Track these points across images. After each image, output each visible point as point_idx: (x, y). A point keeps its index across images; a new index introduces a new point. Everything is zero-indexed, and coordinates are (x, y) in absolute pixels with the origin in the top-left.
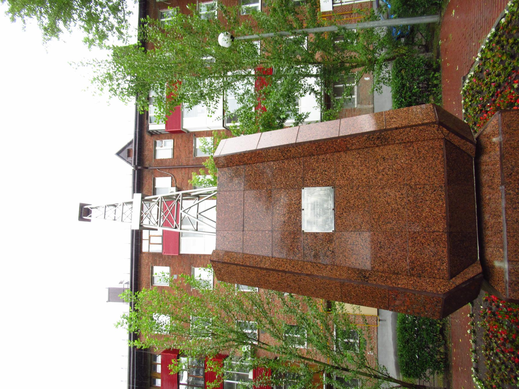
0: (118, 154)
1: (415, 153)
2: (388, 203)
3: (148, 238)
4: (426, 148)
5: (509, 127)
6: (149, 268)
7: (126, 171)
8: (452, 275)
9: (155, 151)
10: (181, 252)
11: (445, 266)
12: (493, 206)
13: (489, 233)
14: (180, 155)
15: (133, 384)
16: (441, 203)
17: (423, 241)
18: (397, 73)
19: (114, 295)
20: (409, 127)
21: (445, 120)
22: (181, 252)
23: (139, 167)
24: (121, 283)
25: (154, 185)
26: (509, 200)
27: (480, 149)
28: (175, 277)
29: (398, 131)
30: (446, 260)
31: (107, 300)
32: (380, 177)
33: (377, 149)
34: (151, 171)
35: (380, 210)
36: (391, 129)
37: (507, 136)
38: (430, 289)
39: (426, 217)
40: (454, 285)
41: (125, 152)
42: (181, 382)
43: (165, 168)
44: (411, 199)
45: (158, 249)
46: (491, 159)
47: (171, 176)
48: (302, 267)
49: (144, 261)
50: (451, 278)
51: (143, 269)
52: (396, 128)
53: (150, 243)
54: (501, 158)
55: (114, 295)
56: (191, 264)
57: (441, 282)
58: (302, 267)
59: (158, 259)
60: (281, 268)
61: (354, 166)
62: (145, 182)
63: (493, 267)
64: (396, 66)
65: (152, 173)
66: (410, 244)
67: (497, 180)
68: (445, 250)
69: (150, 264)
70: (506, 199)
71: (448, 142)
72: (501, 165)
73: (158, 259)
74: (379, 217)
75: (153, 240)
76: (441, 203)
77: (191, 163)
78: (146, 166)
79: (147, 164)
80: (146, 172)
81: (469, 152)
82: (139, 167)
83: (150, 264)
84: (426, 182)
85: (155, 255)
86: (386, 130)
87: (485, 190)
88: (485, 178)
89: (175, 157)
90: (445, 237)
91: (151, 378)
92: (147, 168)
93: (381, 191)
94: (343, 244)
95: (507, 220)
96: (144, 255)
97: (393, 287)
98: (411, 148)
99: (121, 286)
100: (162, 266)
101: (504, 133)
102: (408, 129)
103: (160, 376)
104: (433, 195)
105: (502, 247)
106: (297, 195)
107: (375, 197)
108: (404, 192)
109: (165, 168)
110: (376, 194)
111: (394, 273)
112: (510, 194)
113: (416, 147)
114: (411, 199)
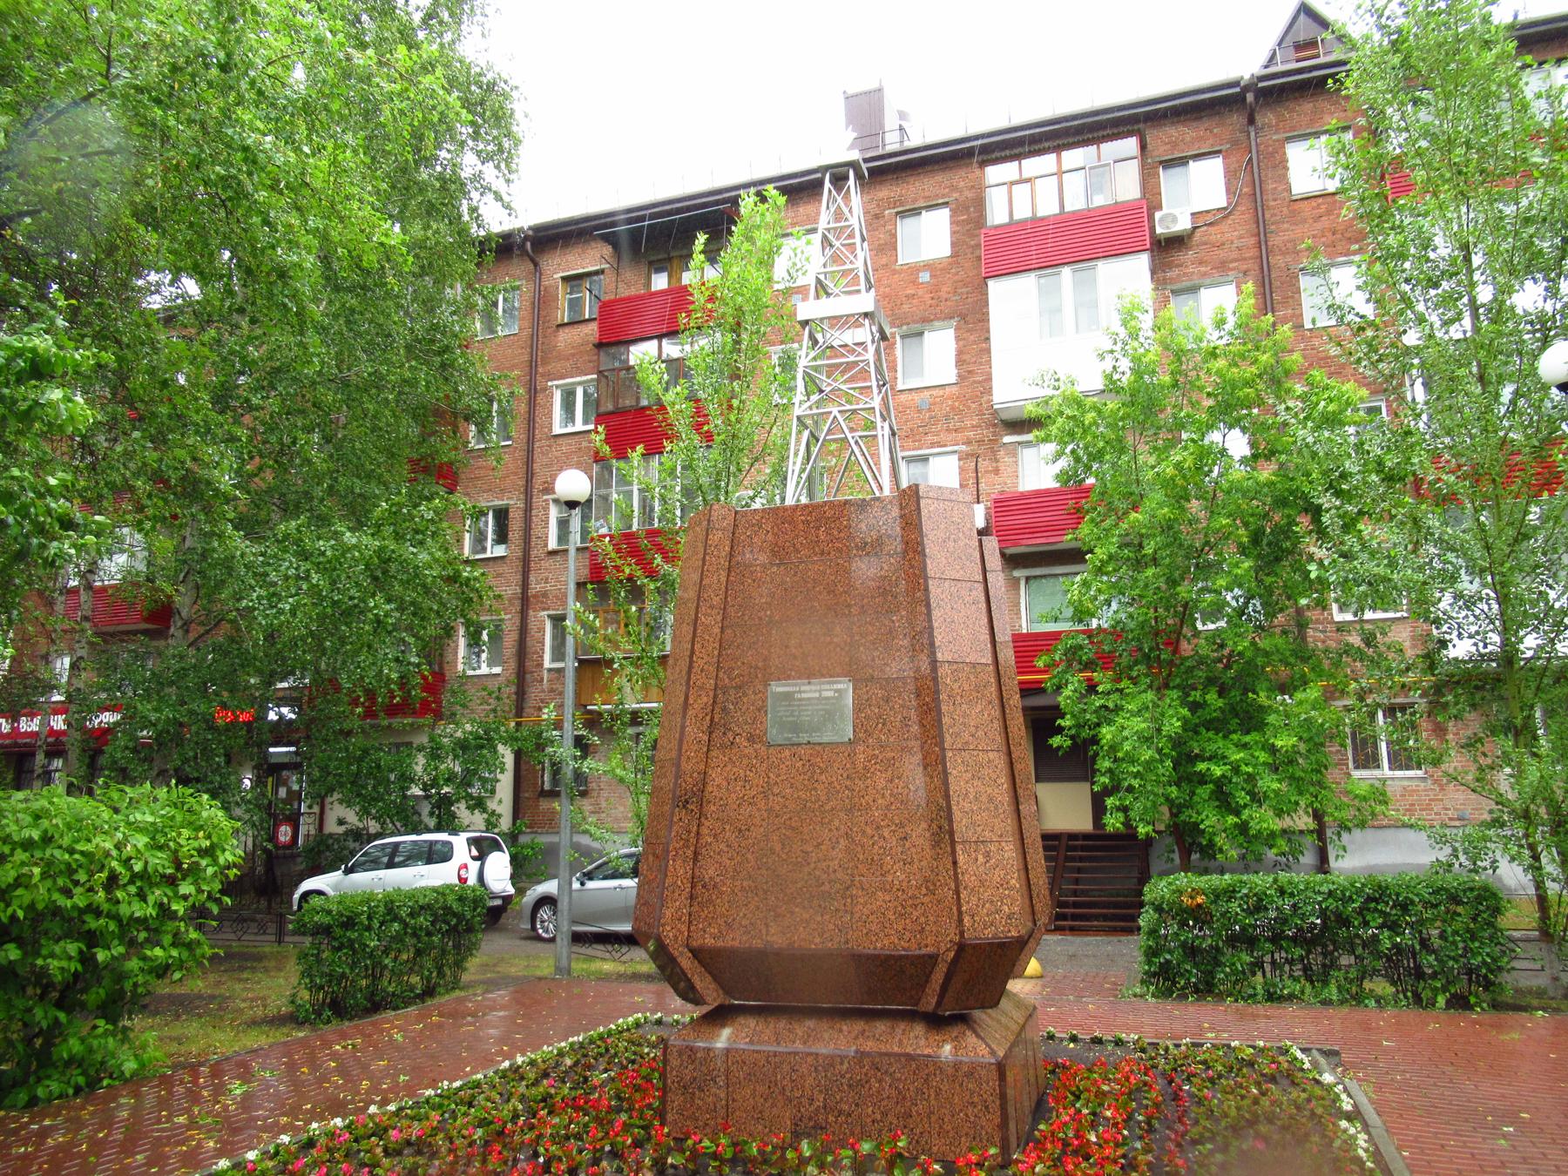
0: (1306, 10)
1: (914, 897)
2: (820, 844)
3: (1025, 176)
4: (923, 919)
5: (970, 1074)
6: (943, 196)
7: (1242, 52)
8: (696, 953)
9: (1317, 135)
10: (991, 283)
11: (709, 941)
12: (826, 1036)
13: (782, 1024)
14: (1304, 221)
15: (652, 217)
16: (817, 940)
17: (752, 906)
18: (1446, 890)
19: (865, 110)
20: (957, 887)
21: (1003, 958)
22: (991, 283)
23: (1250, 97)
24: (902, 115)
25: (1197, 157)
26: (831, 1061)
27: (937, 1022)
28: (925, 277)
29: (950, 866)
30: (720, 944)
31: (851, 92)
32: (869, 831)
33: (924, 825)
34: (1242, 136)
35: (806, 830)
36: (954, 852)
37: (950, 1071)
38: (668, 913)
39: (792, 913)
40: (676, 954)
41: (1305, 29)
42: (664, 341)
43: (1257, 182)
44: (827, 887)
45: (997, 215)
46: (914, 1040)
47: (1229, 204)
48: (701, 688)
49: (959, 178)
50: (691, 951)
51: (939, 177)
52: (955, 863)
53: (1013, 183)
54: (908, 1055)
55: (865, 110)
56: (963, 317)
57: (682, 933)
58: (701, 688)
59: (970, 215)
60: (697, 646)
61: (891, 781)
62: (1206, 123)
63: (723, 1026)
64: (1472, 889)
65: (1235, 143)
66: (745, 884)
67: (869, 1046)
68: (736, 944)
69: (955, 195)
70: (832, 1057)
71: (933, 959)
72: (896, 1055)
73: (970, 215)
74: (793, 829)
75: (1021, 191)
76: (817, 940)
77: (1278, 260)
78: (1257, 117)
79: (1266, 118)
80: (1237, 119)
81: (924, 1000)
82: (1250, 97)
83: (955, 195)
84: (857, 916)
85: (980, 203)
86: (953, 843)
87: (859, 1025)
88: (881, 1027)
89: (1297, 206)
90: (757, 943)
91: (670, 259)
92: (1251, 121)
93: (842, 831)
94: (745, 761)
95: (796, 1054)
96: (978, 172)
97: (668, 852)
98: (924, 891)
99: (891, 122)
100: (953, 233)
101: (957, 1066)
102: (953, 886)
103: (675, 284)
104: (831, 927)
105: (751, 1042)
106: (838, 670)
107: (831, 821)
108: (839, 875)
109: (1257, 182)
110: (836, 823)
111: (696, 853)
112: (842, 1063)
113: (926, 900)
114: (827, 887)
